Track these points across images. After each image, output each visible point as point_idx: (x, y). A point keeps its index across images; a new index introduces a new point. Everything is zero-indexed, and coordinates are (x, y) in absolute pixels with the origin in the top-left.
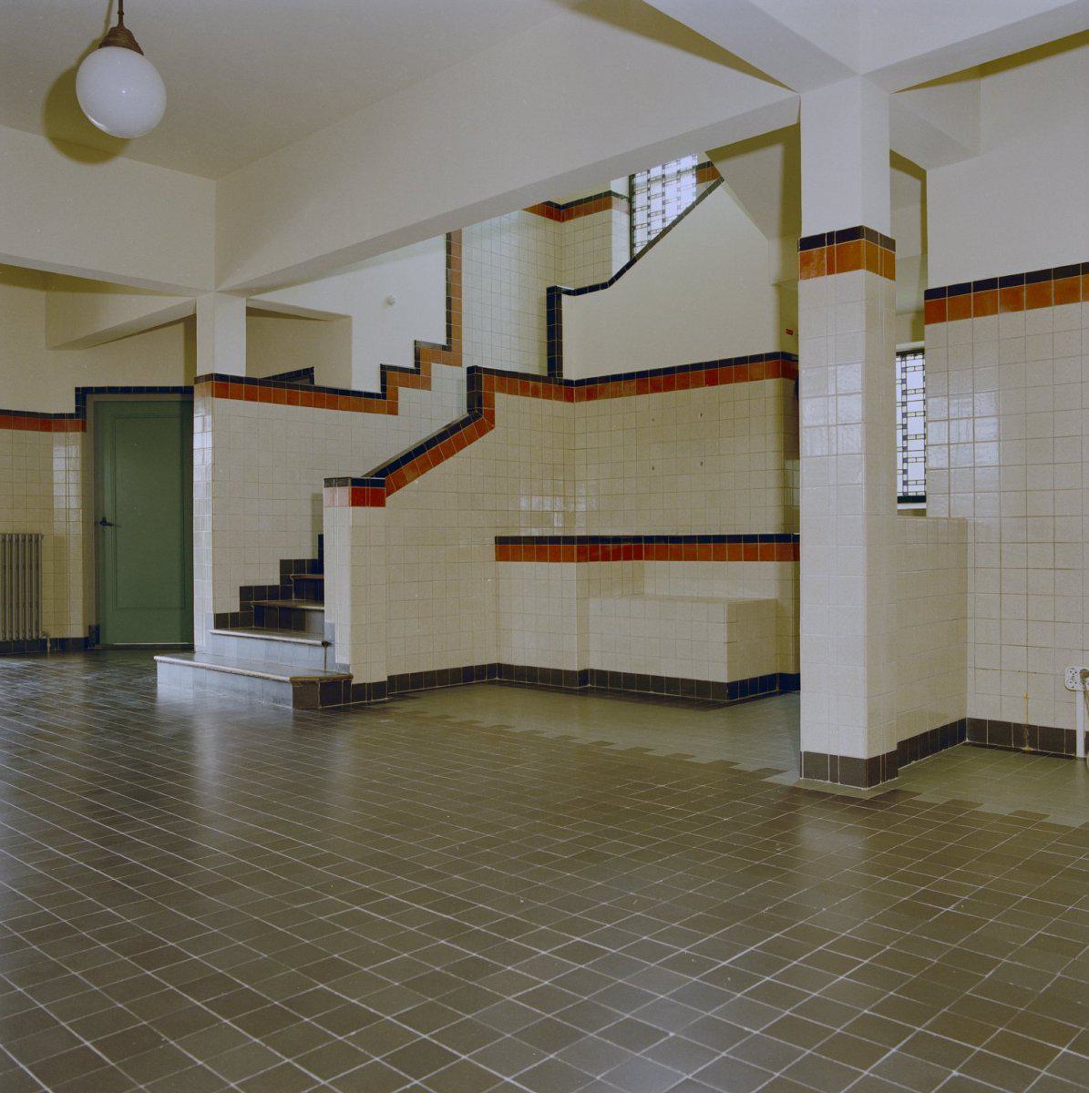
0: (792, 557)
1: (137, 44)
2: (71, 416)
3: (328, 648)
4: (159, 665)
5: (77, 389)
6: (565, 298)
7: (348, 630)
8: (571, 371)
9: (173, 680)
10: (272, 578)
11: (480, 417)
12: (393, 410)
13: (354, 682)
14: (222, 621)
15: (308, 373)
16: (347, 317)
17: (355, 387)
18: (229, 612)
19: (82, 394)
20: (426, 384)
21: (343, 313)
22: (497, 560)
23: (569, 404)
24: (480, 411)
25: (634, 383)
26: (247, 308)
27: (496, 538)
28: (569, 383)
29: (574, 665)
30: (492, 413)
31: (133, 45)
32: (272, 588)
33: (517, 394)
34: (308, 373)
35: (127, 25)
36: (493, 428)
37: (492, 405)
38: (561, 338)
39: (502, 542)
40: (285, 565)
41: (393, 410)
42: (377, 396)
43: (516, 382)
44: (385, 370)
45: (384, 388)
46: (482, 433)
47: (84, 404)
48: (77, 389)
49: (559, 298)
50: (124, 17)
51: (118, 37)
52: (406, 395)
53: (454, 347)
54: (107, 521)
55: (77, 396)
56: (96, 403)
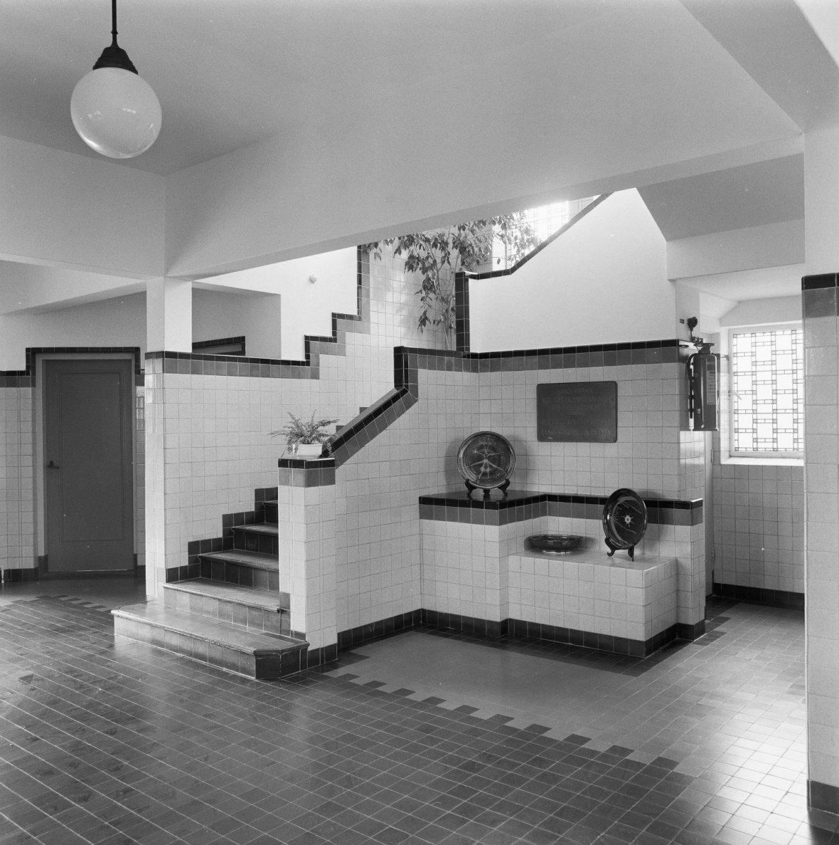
0: (690, 523)
1: (131, 63)
2: (21, 373)
3: (283, 615)
4: (116, 619)
5: (28, 350)
6: (471, 281)
7: (304, 600)
8: (476, 346)
9: (129, 627)
10: (217, 532)
11: (407, 392)
12: (315, 376)
13: (310, 649)
14: (173, 576)
15: (241, 341)
16: (277, 296)
17: (283, 358)
18: (178, 566)
19: (32, 353)
20: (342, 352)
21: (273, 292)
22: (421, 518)
23: (475, 374)
24: (407, 386)
25: (536, 359)
26: (192, 288)
27: (420, 498)
28: (475, 356)
29: (494, 615)
30: (416, 387)
31: (129, 66)
32: (217, 540)
33: (435, 369)
34: (241, 341)
35: (121, 44)
36: (416, 401)
37: (416, 380)
38: (468, 317)
39: (424, 501)
40: (227, 519)
41: (315, 376)
42: (302, 363)
43: (432, 356)
44: (308, 340)
45: (307, 356)
46: (409, 405)
47: (34, 362)
48: (28, 350)
49: (467, 280)
50: (111, 29)
51: (114, 57)
52: (326, 361)
53: (363, 316)
54: (55, 465)
55: (27, 356)
56: (47, 362)
